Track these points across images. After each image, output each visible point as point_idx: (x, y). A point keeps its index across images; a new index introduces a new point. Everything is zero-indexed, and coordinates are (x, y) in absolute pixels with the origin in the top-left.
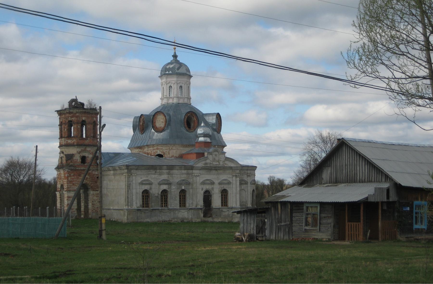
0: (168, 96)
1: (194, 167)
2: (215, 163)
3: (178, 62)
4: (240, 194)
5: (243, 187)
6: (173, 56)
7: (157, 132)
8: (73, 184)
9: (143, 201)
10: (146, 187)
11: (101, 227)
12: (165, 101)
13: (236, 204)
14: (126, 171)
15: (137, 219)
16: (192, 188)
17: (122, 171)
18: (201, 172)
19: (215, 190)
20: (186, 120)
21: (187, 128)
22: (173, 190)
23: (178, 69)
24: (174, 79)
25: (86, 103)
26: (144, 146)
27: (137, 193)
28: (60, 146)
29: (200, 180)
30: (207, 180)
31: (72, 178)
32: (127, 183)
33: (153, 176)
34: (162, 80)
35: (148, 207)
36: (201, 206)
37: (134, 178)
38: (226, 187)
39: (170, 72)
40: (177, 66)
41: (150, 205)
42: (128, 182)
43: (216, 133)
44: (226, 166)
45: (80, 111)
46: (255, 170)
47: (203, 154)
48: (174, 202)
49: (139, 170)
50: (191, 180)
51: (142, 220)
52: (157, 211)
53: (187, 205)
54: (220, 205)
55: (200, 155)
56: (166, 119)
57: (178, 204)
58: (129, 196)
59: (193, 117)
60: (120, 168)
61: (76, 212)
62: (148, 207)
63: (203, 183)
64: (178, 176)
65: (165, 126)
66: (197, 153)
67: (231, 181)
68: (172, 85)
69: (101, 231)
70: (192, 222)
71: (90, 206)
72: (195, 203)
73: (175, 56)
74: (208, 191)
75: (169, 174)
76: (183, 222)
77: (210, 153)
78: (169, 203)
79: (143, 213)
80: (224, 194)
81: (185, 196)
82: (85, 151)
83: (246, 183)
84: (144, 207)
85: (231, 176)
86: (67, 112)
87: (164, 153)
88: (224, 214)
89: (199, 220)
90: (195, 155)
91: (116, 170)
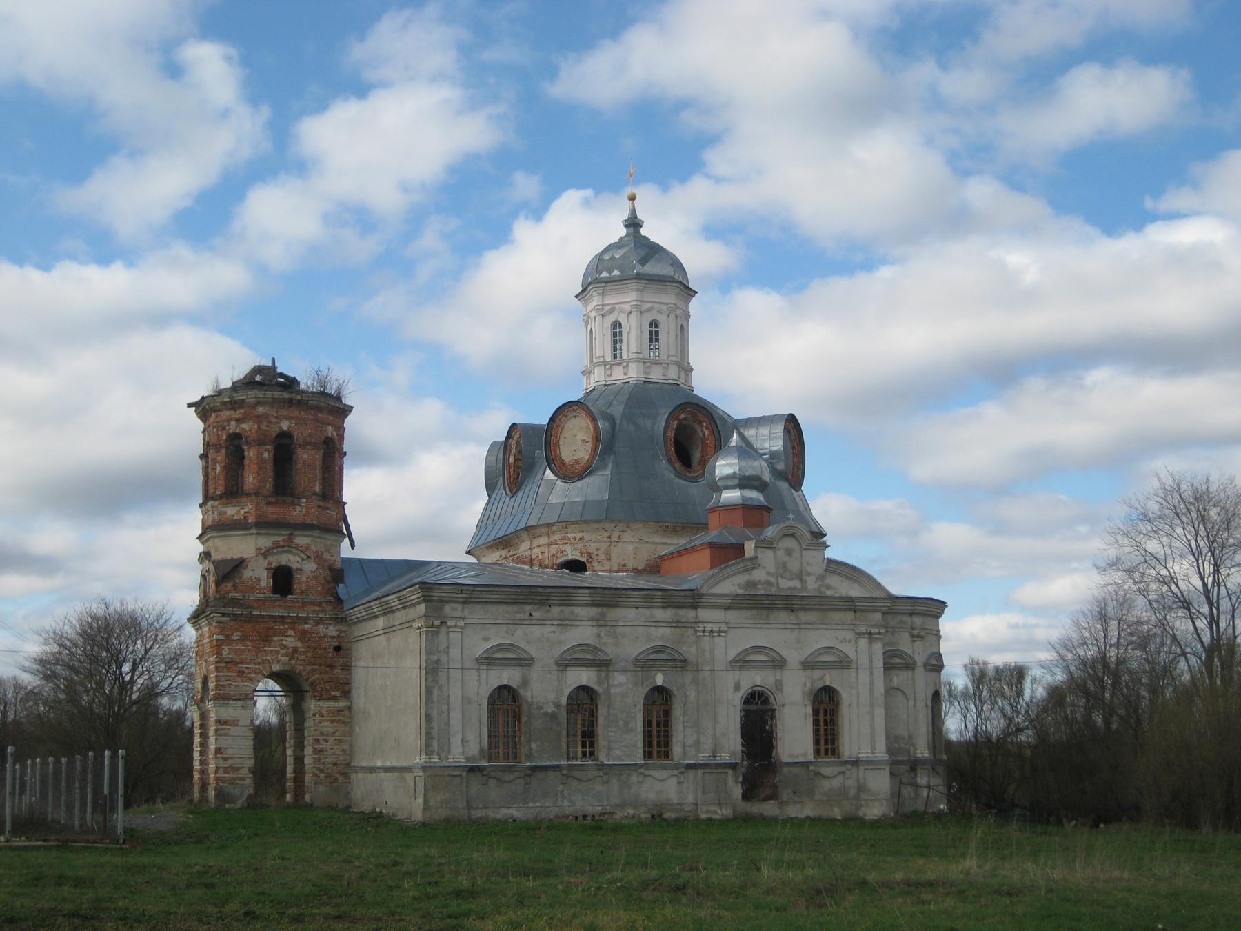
0: (609, 358)
1: (701, 596)
2: (785, 584)
5: (899, 678)
8: (241, 673)
10: (508, 677)
13: (873, 748)
15: (469, 806)
18: (732, 616)
20: (671, 434)
21: (678, 465)
24: (628, 297)
26: (517, 534)
27: (466, 700)
28: (208, 531)
29: (727, 648)
31: (236, 651)
32: (424, 656)
33: (536, 631)
35: (515, 757)
36: (733, 754)
37: (455, 636)
38: (830, 678)
39: (616, 273)
41: (523, 751)
42: (429, 653)
43: (784, 486)
44: (829, 593)
45: (269, 394)
46: (938, 616)
47: (738, 549)
48: (622, 739)
49: (478, 606)
50: (693, 649)
51: (491, 814)
52: (551, 773)
53: (677, 750)
54: (811, 750)
55: (726, 553)
56: (596, 428)
57: (640, 745)
58: (434, 713)
59: (700, 423)
61: (248, 782)
62: (515, 757)
63: (742, 663)
64: (638, 632)
65: (593, 457)
66: (711, 545)
67: (852, 655)
68: (623, 319)
70: (698, 819)
72: (707, 744)
73: (634, 224)
74: (761, 694)
75: (599, 622)
76: (659, 821)
78: (601, 742)
79: (492, 782)
80: (826, 706)
81: (667, 713)
82: (287, 547)
83: (910, 666)
85: (850, 635)
86: (224, 403)
87: (590, 556)
88: (826, 785)
89: (726, 812)
90: (706, 555)
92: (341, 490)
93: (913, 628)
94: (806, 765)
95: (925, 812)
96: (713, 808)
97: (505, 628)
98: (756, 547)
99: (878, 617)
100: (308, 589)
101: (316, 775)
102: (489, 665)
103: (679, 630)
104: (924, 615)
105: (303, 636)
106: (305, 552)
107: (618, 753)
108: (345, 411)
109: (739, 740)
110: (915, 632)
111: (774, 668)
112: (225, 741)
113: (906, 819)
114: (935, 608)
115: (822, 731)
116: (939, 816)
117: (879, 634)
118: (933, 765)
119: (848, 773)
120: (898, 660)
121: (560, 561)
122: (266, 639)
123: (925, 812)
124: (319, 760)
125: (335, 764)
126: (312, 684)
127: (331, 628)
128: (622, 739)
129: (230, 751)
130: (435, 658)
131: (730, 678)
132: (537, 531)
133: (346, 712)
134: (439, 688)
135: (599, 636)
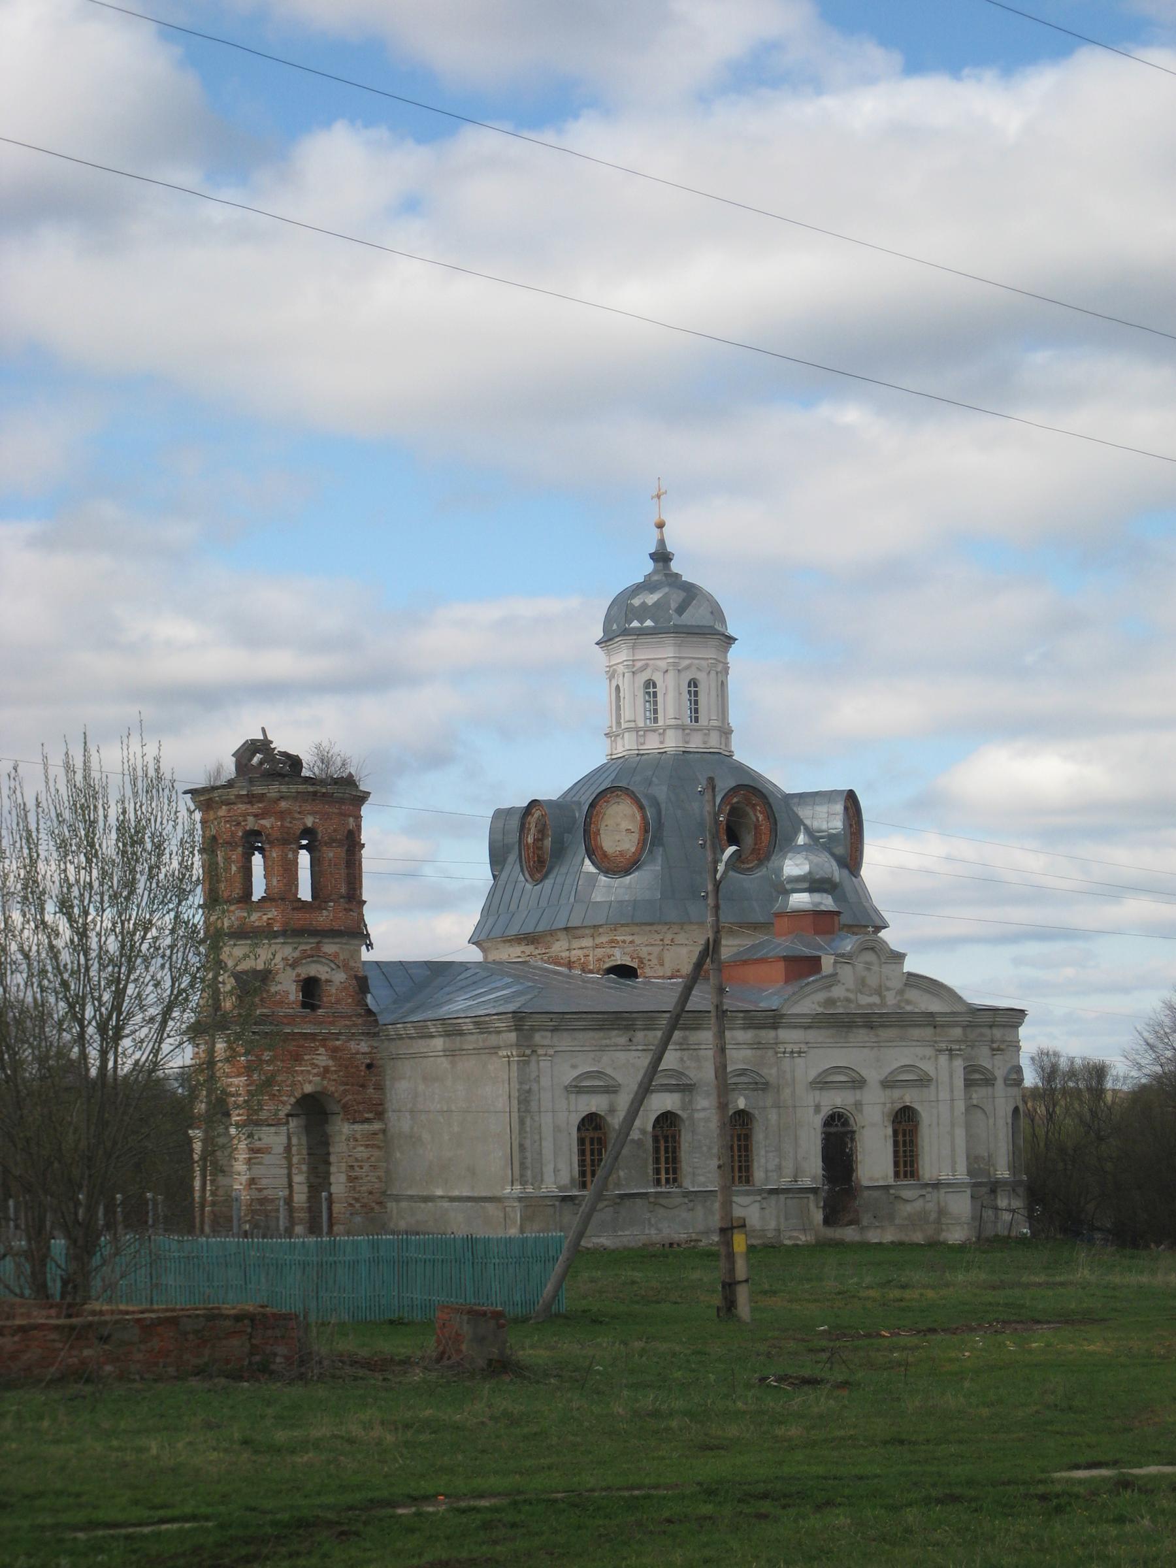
2: (864, 1000)
3: (674, 580)
4: (968, 1126)
5: (978, 1094)
6: (652, 556)
7: (606, 872)
9: (582, 1163)
10: (595, 1104)
11: (732, 1270)
12: (626, 745)
13: (954, 1170)
14: (512, 1036)
16: (777, 1106)
17: (493, 1040)
18: (812, 1035)
19: (867, 1110)
22: (701, 1115)
23: (681, 610)
24: (663, 654)
25: (307, 758)
26: (552, 933)
27: (557, 1129)
29: (807, 1069)
30: (837, 1069)
33: (622, 1056)
34: (609, 654)
38: (909, 1097)
40: (677, 597)
44: (909, 1008)
46: (1016, 1026)
47: (812, 964)
48: (702, 1165)
49: (565, 1034)
50: (774, 1071)
53: (758, 1175)
54: (891, 1173)
55: (803, 967)
56: (644, 817)
58: (528, 1143)
59: (754, 806)
60: (481, 1025)
62: (912, 1176)
63: (821, 1083)
66: (787, 959)
67: (932, 1073)
68: (658, 678)
69: (729, 1286)
71: (339, 1184)
72: (789, 1167)
73: (662, 557)
77: (844, 959)
78: (685, 1166)
80: (905, 1123)
82: (315, 956)
83: (989, 1081)
84: (658, 1182)
86: (239, 796)
91: (461, 1033)
92: (361, 887)
93: (993, 1041)
94: (886, 1188)
95: (1009, 1237)
96: (795, 1234)
97: (592, 1055)
98: (836, 962)
99: (957, 1032)
100: (338, 1002)
101: (351, 1205)
102: (578, 1093)
103: (759, 1052)
104: (1004, 1026)
105: (334, 1052)
106: (332, 959)
107: (702, 1179)
108: (363, 798)
109: (820, 1163)
110: (995, 1046)
111: (854, 1088)
112: (258, 1171)
113: (989, 1243)
114: (1016, 1017)
115: (901, 1154)
116: (1022, 1241)
117: (960, 1050)
118: (1013, 1187)
119: (928, 1197)
120: (977, 1076)
121: (607, 966)
122: (297, 1058)
123: (1009, 1237)
124: (354, 1188)
125: (370, 1193)
126: (345, 1107)
127: (363, 1044)
128: (702, 1165)
129: (264, 1182)
130: (527, 1087)
131: (810, 1098)
132: (579, 932)
133: (381, 1136)
134: (532, 1118)
135: (682, 1059)
